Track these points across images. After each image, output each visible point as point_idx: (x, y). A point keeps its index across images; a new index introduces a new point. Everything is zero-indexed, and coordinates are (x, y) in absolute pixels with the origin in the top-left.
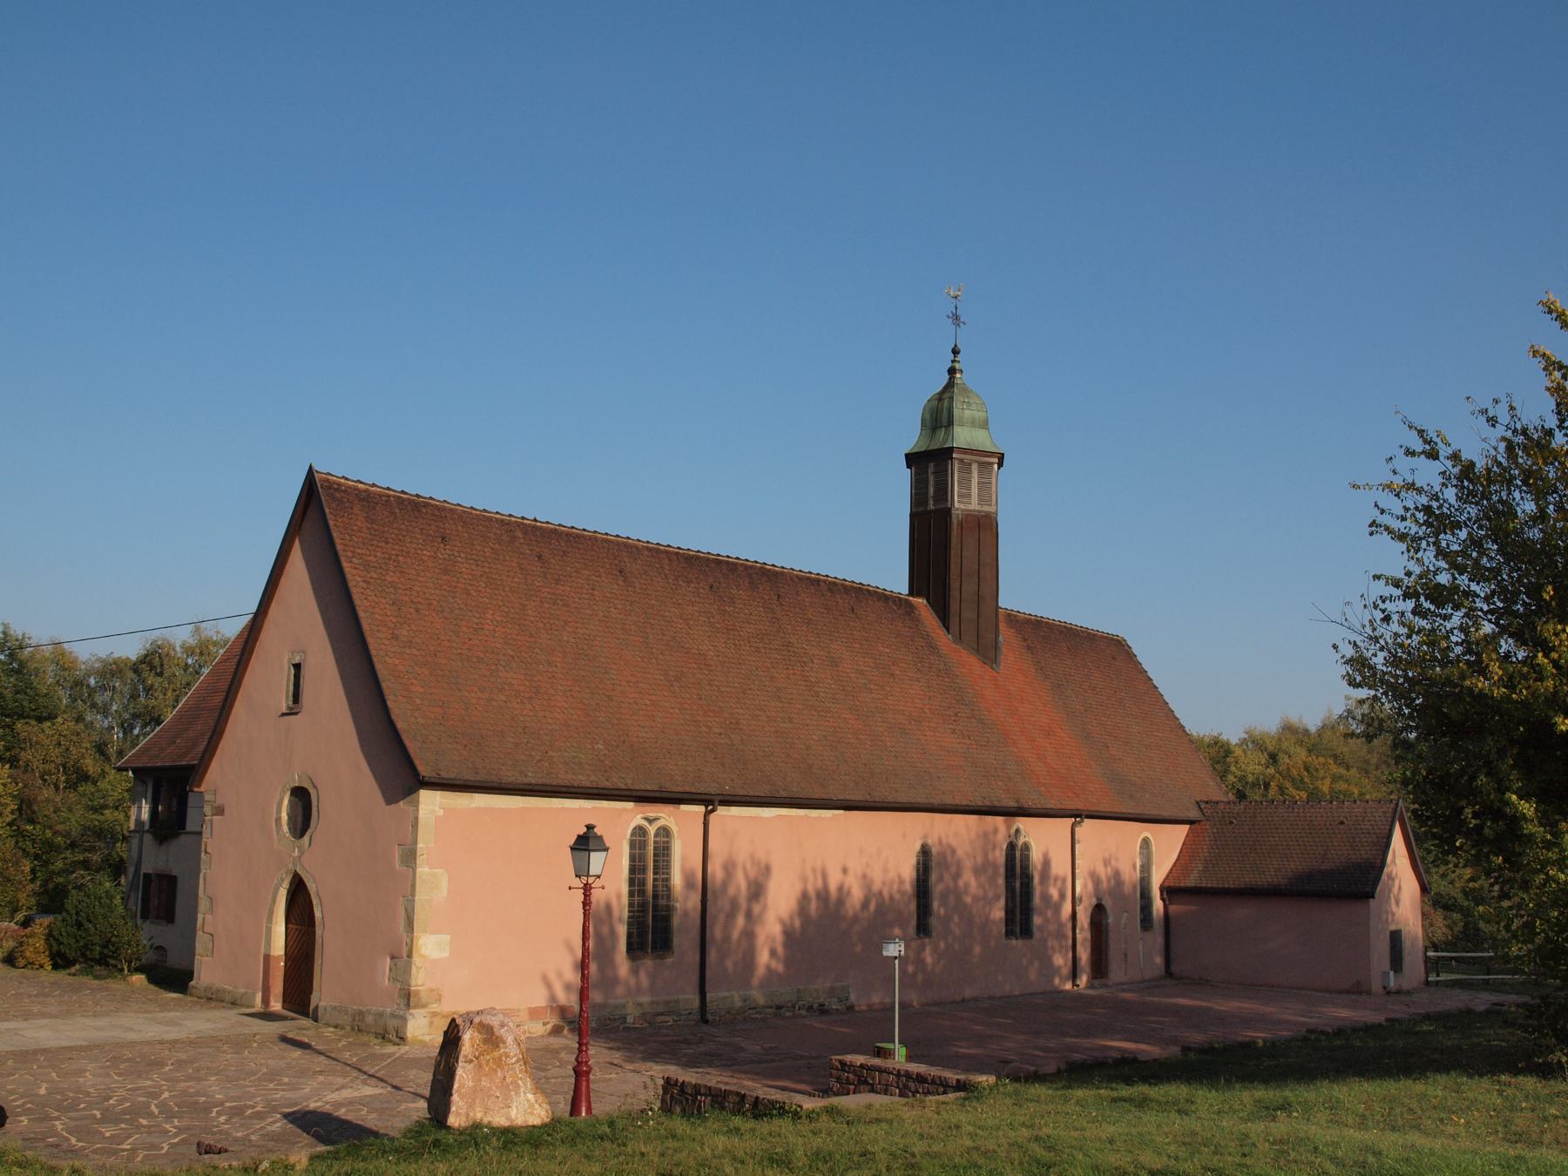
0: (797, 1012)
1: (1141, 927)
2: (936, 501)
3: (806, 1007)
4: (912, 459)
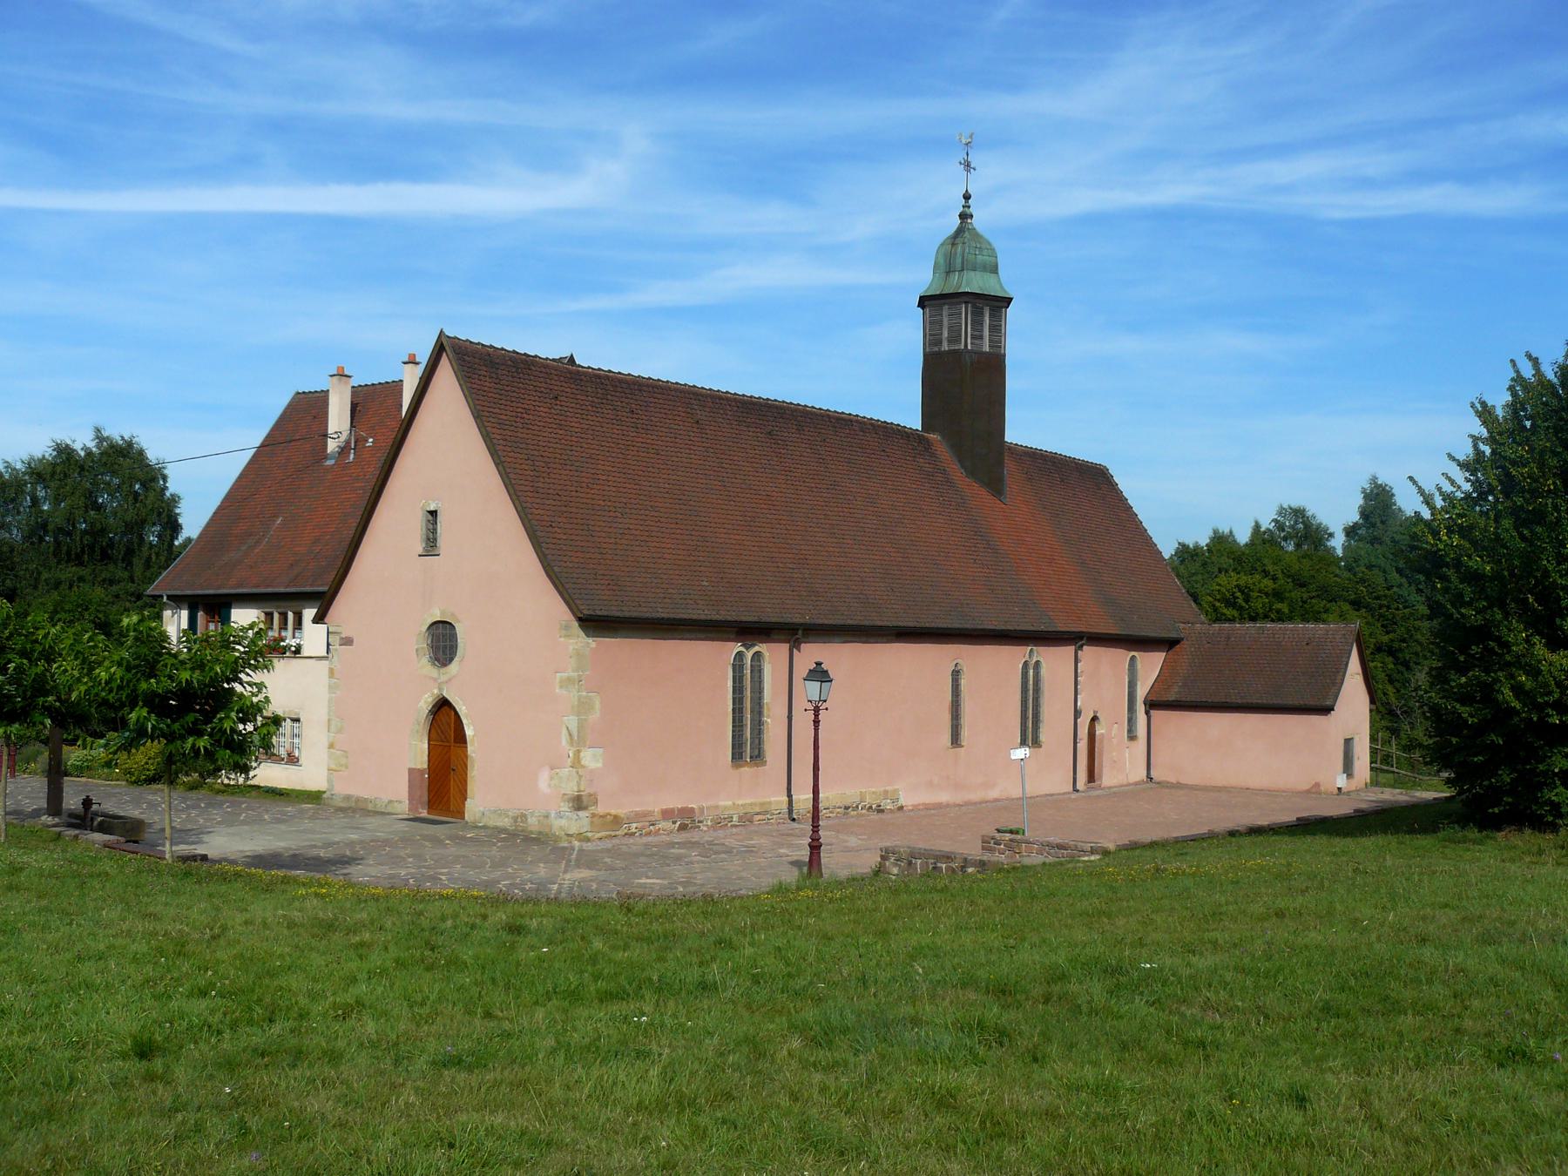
2: (950, 341)
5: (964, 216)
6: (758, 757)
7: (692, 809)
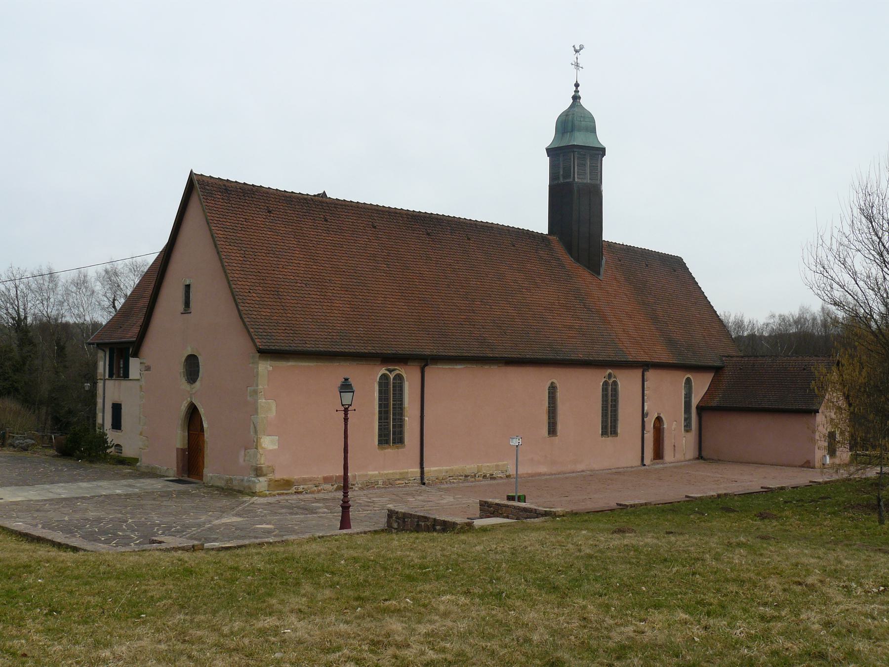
0: (476, 478)
2: (564, 177)
4: (550, 151)
6: (399, 440)
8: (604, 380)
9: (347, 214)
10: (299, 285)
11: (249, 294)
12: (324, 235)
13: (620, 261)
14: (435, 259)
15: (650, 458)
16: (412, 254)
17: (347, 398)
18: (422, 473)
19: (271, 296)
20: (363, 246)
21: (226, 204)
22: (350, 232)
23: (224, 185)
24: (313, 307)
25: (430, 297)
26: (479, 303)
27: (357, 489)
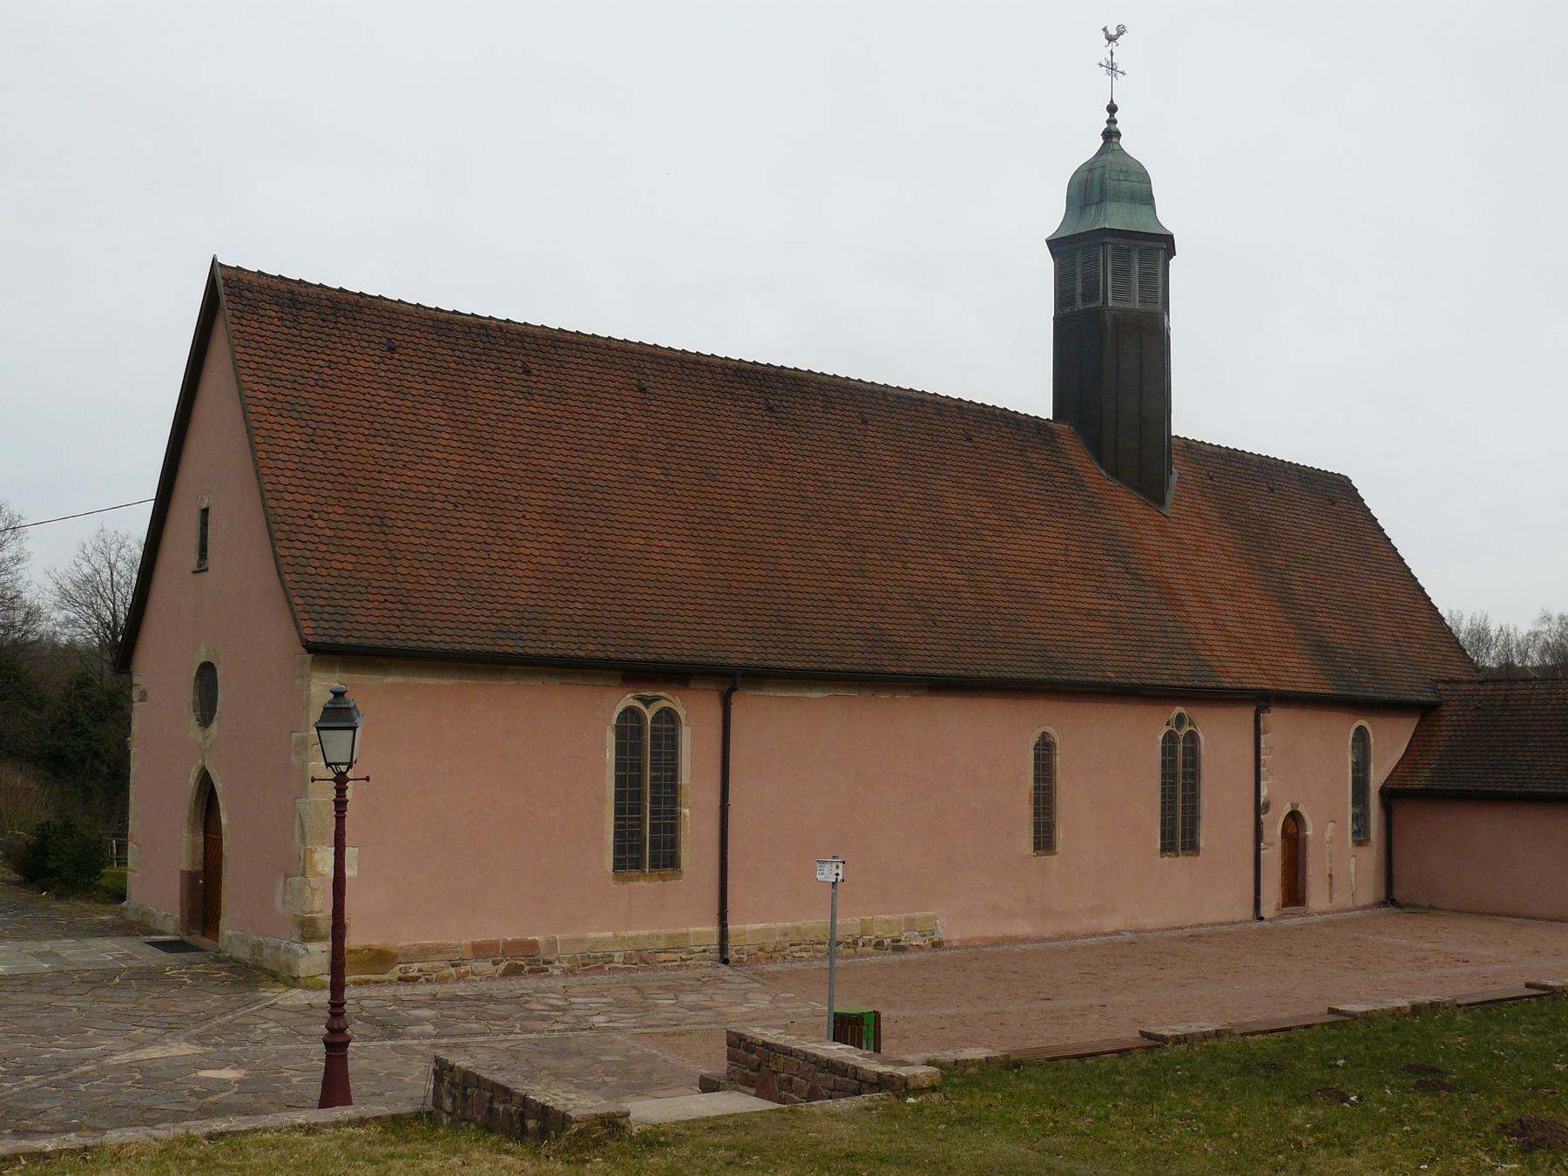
1: (1353, 841)
2: (1085, 299)
3: (873, 943)
4: (1056, 245)
5: (1111, 135)
6: (666, 859)
7: (534, 944)
8: (1166, 729)
9: (580, 361)
10: (438, 505)
11: (309, 522)
12: (518, 401)
13: (1211, 478)
14: (780, 461)
15: (1275, 903)
16: (727, 449)
17: (338, 743)
18: (723, 935)
19: (365, 528)
20: (609, 427)
21: (286, 331)
22: (581, 398)
23: (292, 292)
24: (464, 553)
25: (759, 539)
26: (878, 557)
27: (557, 972)
